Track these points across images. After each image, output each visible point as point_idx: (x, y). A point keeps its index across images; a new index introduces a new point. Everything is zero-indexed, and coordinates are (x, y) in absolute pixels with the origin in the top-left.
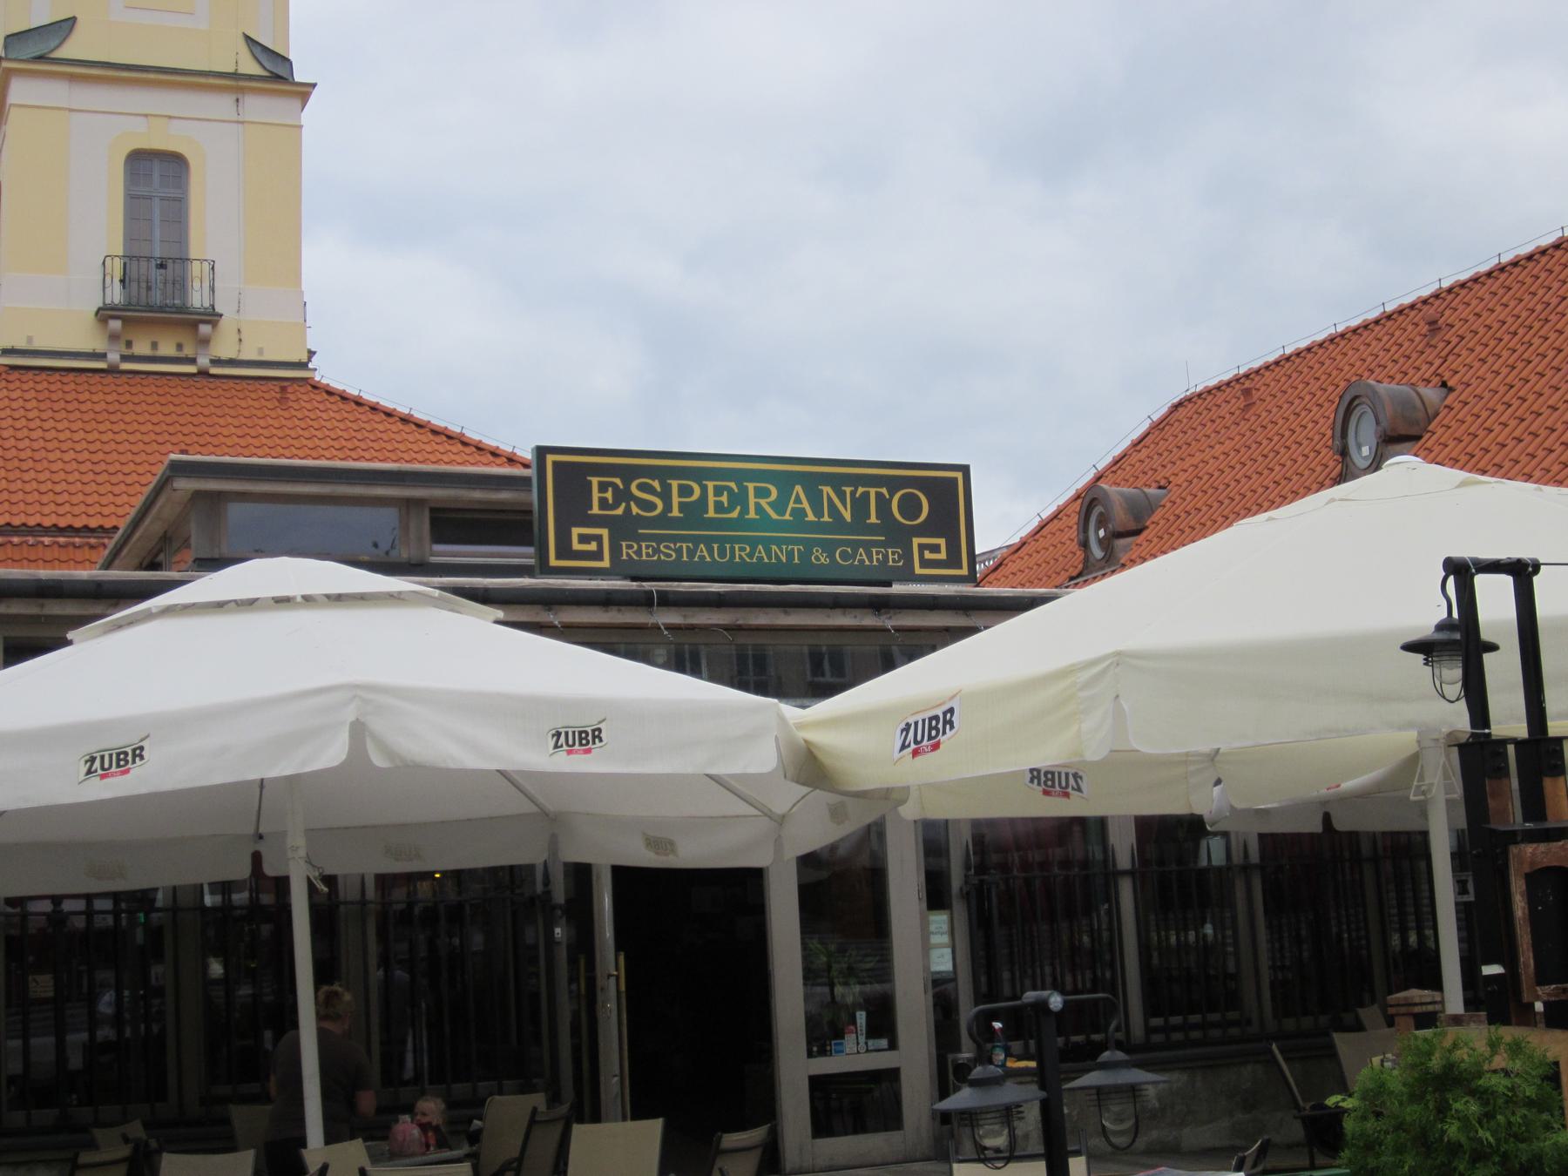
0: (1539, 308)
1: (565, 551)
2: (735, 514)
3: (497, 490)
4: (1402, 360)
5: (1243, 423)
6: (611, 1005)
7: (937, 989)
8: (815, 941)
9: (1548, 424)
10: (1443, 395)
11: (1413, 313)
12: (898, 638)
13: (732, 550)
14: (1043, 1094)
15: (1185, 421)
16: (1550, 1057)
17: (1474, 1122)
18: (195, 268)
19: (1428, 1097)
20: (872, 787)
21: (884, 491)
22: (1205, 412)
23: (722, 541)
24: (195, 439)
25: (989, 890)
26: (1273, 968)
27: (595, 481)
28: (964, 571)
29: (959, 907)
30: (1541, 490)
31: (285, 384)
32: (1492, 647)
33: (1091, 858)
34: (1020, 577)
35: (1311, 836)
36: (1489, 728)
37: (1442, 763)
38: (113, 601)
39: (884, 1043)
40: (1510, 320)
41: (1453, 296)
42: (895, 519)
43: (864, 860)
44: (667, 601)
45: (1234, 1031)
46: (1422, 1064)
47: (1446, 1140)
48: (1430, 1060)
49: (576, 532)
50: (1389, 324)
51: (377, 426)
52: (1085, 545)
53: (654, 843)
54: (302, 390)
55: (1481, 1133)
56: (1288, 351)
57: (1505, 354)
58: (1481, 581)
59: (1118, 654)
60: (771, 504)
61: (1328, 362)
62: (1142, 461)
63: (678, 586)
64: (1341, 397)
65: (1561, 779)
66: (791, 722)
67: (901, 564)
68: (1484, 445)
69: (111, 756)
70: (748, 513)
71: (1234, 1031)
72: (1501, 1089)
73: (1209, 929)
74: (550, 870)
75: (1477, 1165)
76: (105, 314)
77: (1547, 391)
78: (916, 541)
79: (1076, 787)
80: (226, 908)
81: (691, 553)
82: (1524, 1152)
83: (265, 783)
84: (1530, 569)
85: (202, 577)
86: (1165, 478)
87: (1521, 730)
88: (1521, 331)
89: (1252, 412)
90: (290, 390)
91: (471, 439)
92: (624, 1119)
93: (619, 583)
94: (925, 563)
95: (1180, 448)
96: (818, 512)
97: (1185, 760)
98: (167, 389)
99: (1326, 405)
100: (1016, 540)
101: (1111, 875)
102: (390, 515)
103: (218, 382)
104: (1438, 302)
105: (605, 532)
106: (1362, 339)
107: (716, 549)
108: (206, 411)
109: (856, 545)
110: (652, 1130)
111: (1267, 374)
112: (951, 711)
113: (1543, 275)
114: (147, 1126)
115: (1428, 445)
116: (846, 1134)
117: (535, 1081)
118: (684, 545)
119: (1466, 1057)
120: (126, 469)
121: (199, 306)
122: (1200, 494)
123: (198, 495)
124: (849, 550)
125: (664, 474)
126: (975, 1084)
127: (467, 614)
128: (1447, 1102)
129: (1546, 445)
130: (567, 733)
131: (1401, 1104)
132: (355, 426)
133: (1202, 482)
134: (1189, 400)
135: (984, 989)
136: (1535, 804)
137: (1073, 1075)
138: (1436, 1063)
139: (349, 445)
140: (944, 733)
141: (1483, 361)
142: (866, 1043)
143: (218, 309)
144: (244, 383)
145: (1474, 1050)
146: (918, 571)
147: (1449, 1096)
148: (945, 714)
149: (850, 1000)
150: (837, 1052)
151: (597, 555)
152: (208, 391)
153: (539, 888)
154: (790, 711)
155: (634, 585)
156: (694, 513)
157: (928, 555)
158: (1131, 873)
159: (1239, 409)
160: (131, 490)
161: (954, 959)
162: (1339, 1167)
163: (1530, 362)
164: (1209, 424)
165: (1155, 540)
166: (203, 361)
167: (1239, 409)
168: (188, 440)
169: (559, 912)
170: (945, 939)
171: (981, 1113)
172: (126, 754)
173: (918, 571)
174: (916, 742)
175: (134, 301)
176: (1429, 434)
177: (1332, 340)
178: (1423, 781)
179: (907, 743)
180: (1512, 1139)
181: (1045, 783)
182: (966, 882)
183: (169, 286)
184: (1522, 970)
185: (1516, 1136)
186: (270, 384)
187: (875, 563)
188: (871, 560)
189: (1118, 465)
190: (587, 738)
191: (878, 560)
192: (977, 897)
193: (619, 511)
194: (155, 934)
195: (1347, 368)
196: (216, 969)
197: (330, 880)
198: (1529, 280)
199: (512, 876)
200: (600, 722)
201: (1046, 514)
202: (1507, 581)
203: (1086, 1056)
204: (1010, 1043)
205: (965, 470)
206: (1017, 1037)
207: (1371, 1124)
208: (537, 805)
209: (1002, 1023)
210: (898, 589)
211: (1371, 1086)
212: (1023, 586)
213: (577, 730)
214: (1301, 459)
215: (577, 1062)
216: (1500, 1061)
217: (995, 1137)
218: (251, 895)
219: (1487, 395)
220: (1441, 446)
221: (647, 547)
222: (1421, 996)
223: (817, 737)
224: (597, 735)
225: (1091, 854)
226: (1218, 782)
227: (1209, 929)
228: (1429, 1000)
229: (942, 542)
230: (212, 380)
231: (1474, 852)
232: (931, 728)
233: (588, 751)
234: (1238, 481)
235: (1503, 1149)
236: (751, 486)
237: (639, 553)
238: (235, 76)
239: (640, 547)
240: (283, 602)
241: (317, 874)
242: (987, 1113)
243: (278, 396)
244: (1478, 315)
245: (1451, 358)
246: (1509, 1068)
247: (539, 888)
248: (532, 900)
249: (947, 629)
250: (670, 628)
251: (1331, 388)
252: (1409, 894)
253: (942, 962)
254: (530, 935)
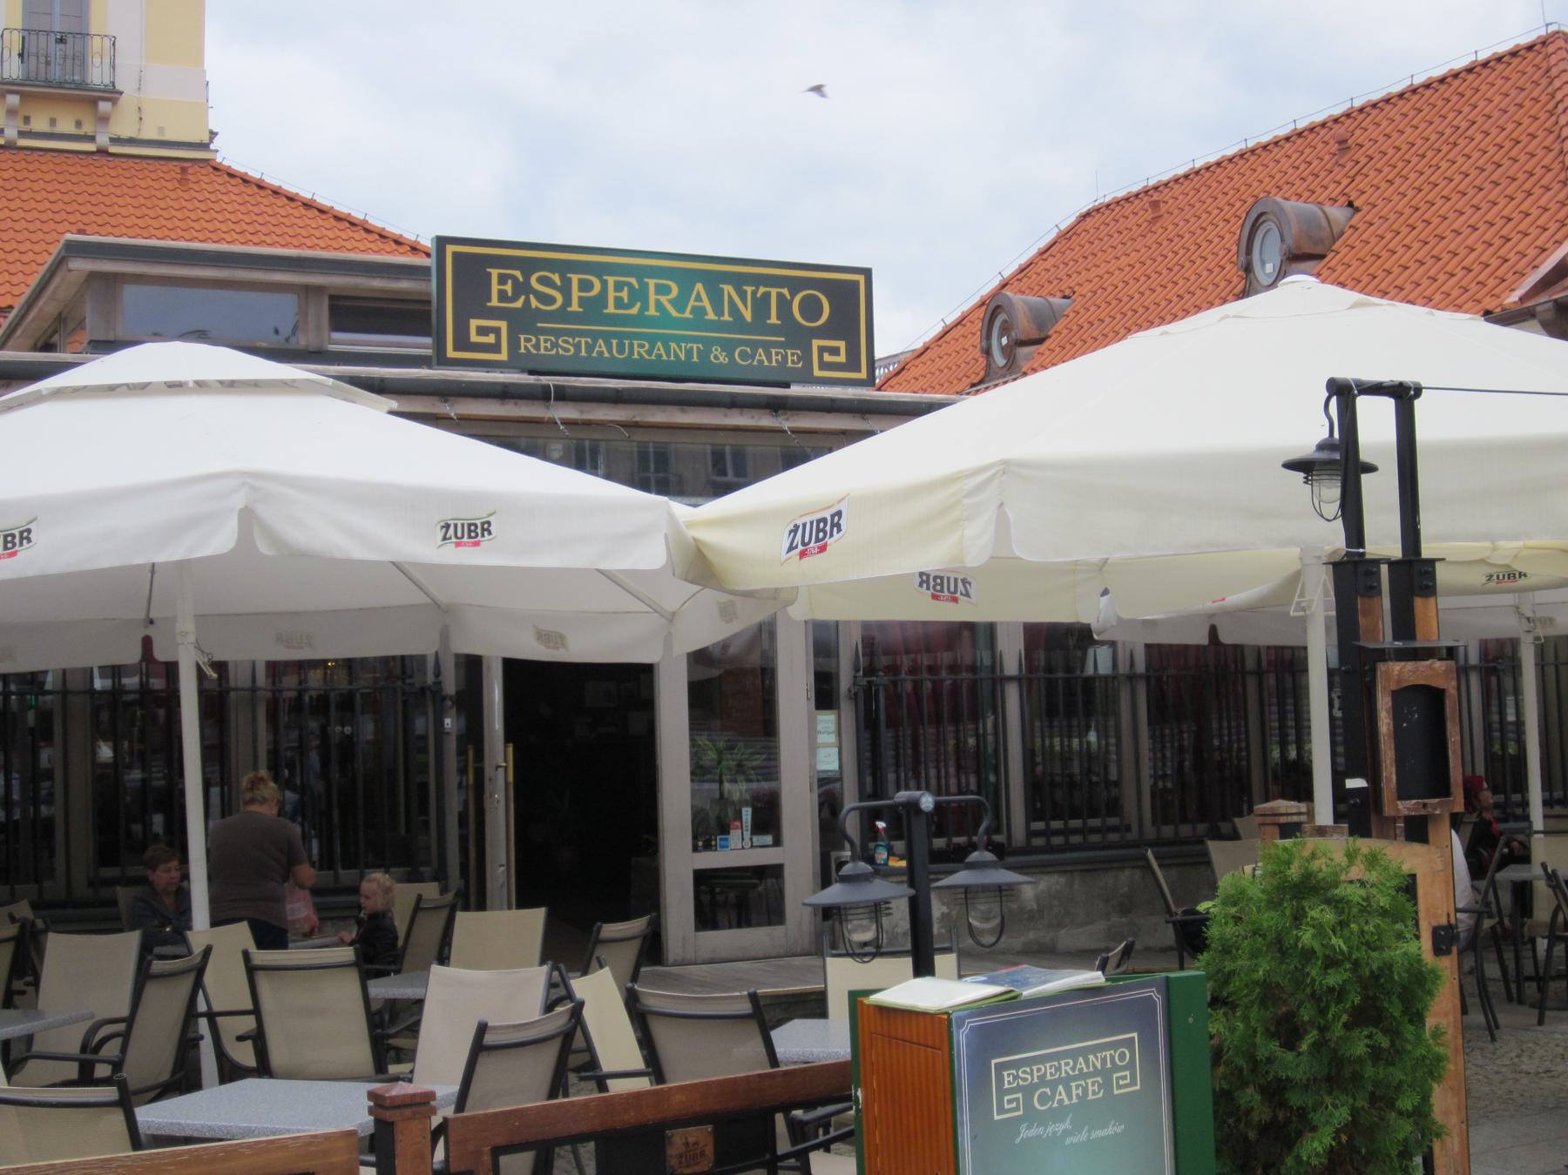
0: (1448, 131)
1: (462, 343)
2: (634, 311)
3: (398, 279)
4: (1310, 179)
5: (1149, 235)
6: (499, 796)
7: (824, 788)
8: (704, 738)
9: (1451, 247)
10: (1349, 215)
11: (1323, 132)
12: (794, 439)
13: (631, 346)
14: (912, 892)
15: (1092, 231)
16: (1406, 868)
17: (1328, 930)
18: (96, 43)
19: (1285, 905)
20: (758, 587)
21: (785, 291)
22: (1112, 223)
23: (620, 336)
24: (93, 218)
25: (877, 691)
26: (1155, 777)
27: (495, 273)
28: (863, 375)
29: (847, 707)
30: (1433, 315)
31: (186, 165)
32: (1370, 469)
33: (979, 664)
34: (922, 382)
35: (1197, 647)
36: (1363, 547)
37: (1322, 582)
38: (6, 381)
39: (769, 839)
40: (1419, 142)
41: (1363, 115)
42: (795, 319)
43: (755, 660)
44: (563, 395)
45: (1114, 837)
46: (1281, 872)
47: (1300, 946)
48: (1289, 868)
49: (474, 323)
50: (1300, 141)
51: (279, 210)
52: (987, 352)
53: (544, 637)
54: (203, 171)
55: (1334, 941)
56: (1198, 165)
57: (1413, 176)
58: (1363, 403)
59: (1005, 463)
61: (1237, 177)
62: (1048, 270)
63: (575, 381)
64: (1247, 213)
65: (1432, 600)
66: (681, 520)
67: (800, 365)
68: (1386, 266)
70: (648, 309)
71: (1114, 837)
72: (1356, 899)
73: (1092, 737)
74: (441, 662)
75: (1329, 971)
77: (1452, 215)
78: (816, 343)
79: (964, 592)
80: (117, 692)
81: (590, 348)
82: (1376, 960)
83: (156, 568)
84: (1412, 393)
85: (94, 360)
86: (1070, 288)
87: (1395, 550)
88: (1430, 154)
89: (1159, 224)
90: (190, 171)
91: (374, 226)
92: (510, 908)
93: (516, 376)
94: (824, 366)
95: (1086, 258)
96: (718, 311)
97: (1074, 568)
98: (66, 168)
99: (1233, 220)
100: (919, 345)
101: (998, 681)
102: (289, 302)
103: (117, 161)
104: (1348, 122)
105: (503, 325)
106: (1272, 155)
107: (614, 345)
108: (105, 191)
109: (755, 345)
110: (536, 917)
111: (1176, 186)
112: (839, 514)
113: (1454, 98)
114: (34, 906)
115: (1332, 264)
116: (730, 927)
117: (421, 869)
118: (583, 340)
119: (1324, 867)
120: (22, 248)
121: (99, 83)
122: (1103, 305)
123: (93, 276)
124: (748, 349)
126: (845, 879)
127: (361, 404)
128: (1303, 909)
129: (1448, 269)
130: (456, 526)
131: (1259, 910)
132: (256, 210)
133: (1107, 293)
134: (1098, 210)
135: (869, 789)
136: (1405, 623)
137: (939, 876)
138: (1294, 872)
139: (251, 229)
140: (831, 535)
141: (1391, 182)
142: (751, 839)
143: (119, 87)
144: (144, 163)
145: (1331, 860)
146: (817, 373)
147: (1306, 904)
148: (833, 516)
149: (736, 797)
150: (722, 847)
151: (495, 348)
152: (107, 170)
153: (430, 679)
154: (679, 509)
155: (532, 379)
156: (594, 308)
157: (827, 358)
158: (1018, 679)
159: (1146, 221)
160: (27, 269)
161: (840, 759)
162: (1198, 969)
163: (1436, 185)
164: (1116, 235)
165: (1058, 349)
166: (103, 140)
167: (1146, 221)
168: (85, 219)
169: (449, 703)
170: (832, 738)
171: (850, 908)
172: (13, 536)
173: (817, 373)
174: (804, 544)
175: (33, 76)
176: (1333, 254)
177: (1242, 155)
178: (1304, 597)
179: (794, 545)
180: (1364, 948)
181: (934, 587)
182: (854, 684)
183: (69, 62)
184: (1384, 785)
185: (1367, 944)
186: (171, 164)
187: (774, 364)
188: (770, 360)
189: (1025, 272)
190: (476, 531)
191: (777, 361)
192: (866, 698)
193: (519, 304)
194: (45, 717)
195: (1255, 184)
196: (106, 752)
197: (221, 667)
198: (1440, 103)
199: (400, 669)
200: (490, 515)
201: (950, 320)
202: (1387, 405)
203: (956, 857)
204: (892, 843)
205: (867, 273)
206: (899, 837)
207: (1230, 930)
208: (429, 596)
209: (886, 822)
210: (796, 390)
211: (1233, 892)
212: (925, 391)
213: (466, 522)
214: (1205, 274)
215: (464, 850)
216: (1356, 872)
217: (864, 931)
218: (141, 679)
219: (1392, 216)
220: (1344, 267)
221: (546, 341)
222: (1287, 807)
223: (707, 536)
224: (486, 528)
225: (979, 659)
226: (1105, 592)
227: (1092, 737)
228: (1294, 811)
229: (842, 345)
230: (111, 159)
231: (1343, 668)
232: (818, 531)
233: (477, 544)
234: (1142, 294)
235: (1354, 957)
236: (652, 283)
237: (537, 346)
239: (538, 341)
240: (175, 387)
241: (206, 659)
242: (856, 908)
243: (179, 177)
244: (1388, 136)
245: (1358, 178)
246: (1366, 878)
247: (430, 679)
248: (423, 690)
249: (844, 432)
250: (566, 422)
251: (1238, 204)
252: (1290, 708)
253: (828, 761)
254: (420, 725)
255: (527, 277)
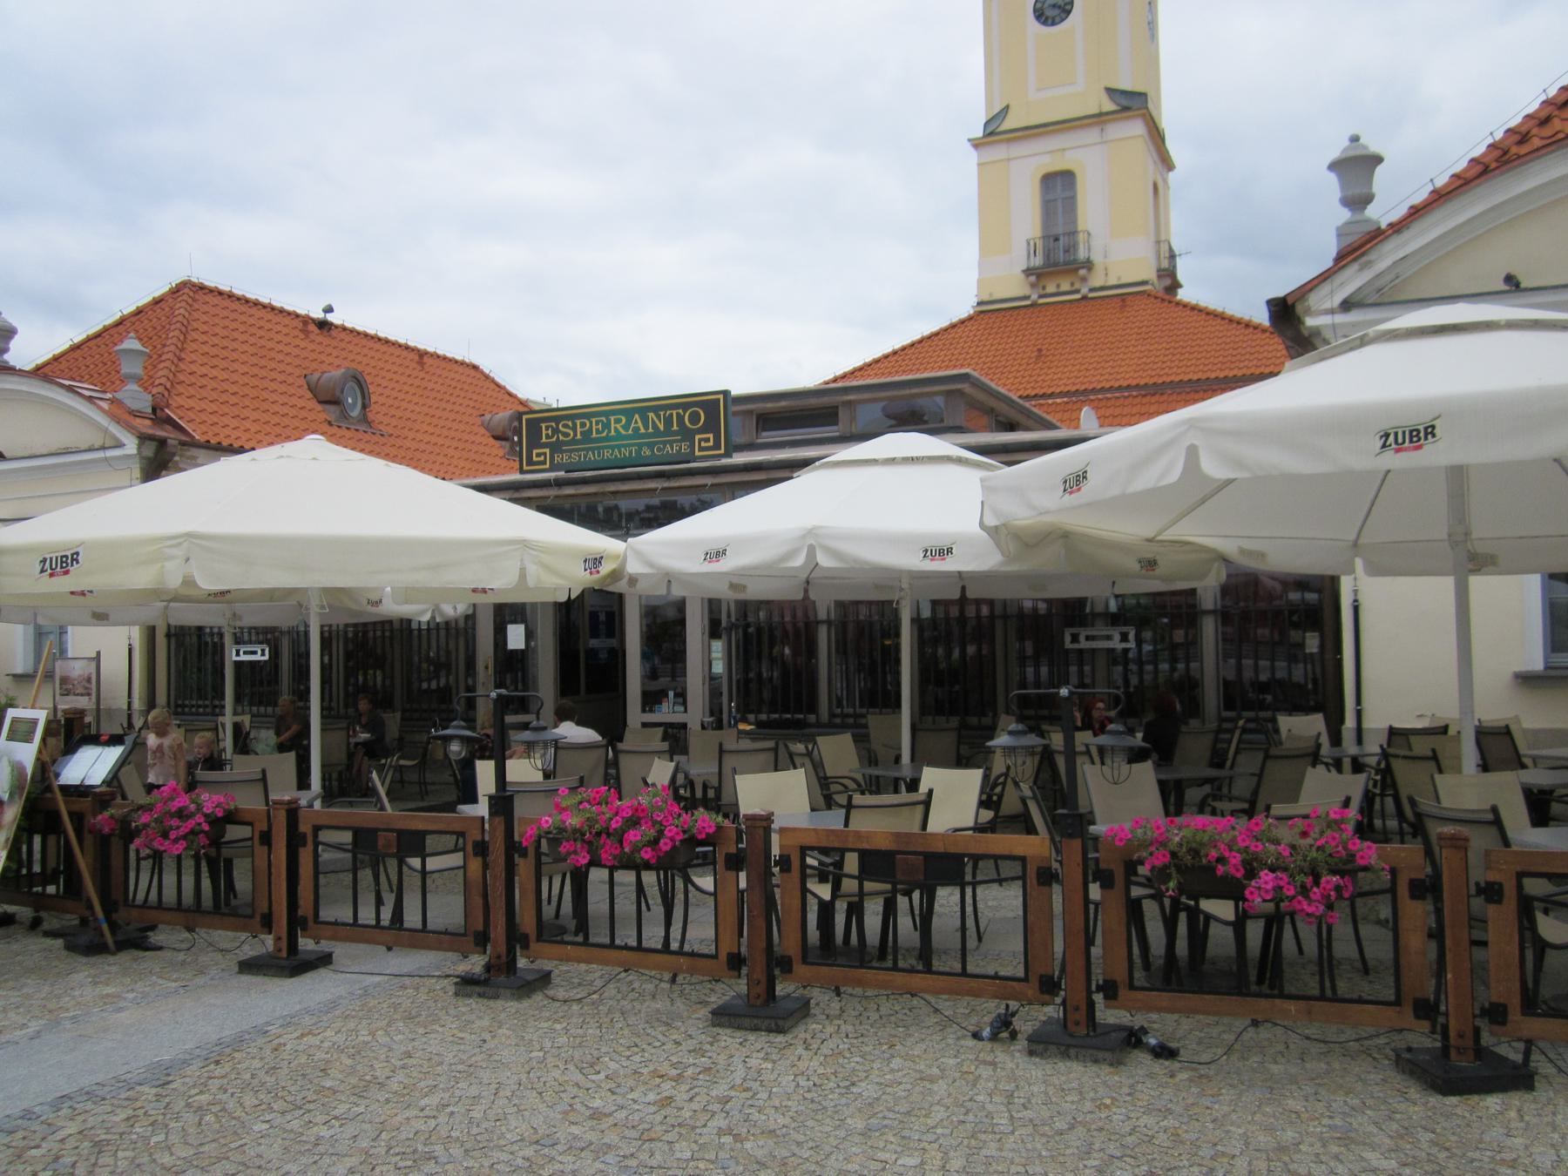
23: (599, 448)
49: (535, 452)
60: (622, 427)
69: (1404, 432)
76: (1028, 272)
81: (585, 457)
94: (701, 449)
96: (646, 427)
105: (547, 451)
109: (665, 443)
125: (573, 417)
156: (587, 435)
157: (703, 444)
158: (829, 622)
166: (1084, 291)
172: (1418, 431)
229: (711, 436)
238: (1101, 114)
255: (557, 425)
